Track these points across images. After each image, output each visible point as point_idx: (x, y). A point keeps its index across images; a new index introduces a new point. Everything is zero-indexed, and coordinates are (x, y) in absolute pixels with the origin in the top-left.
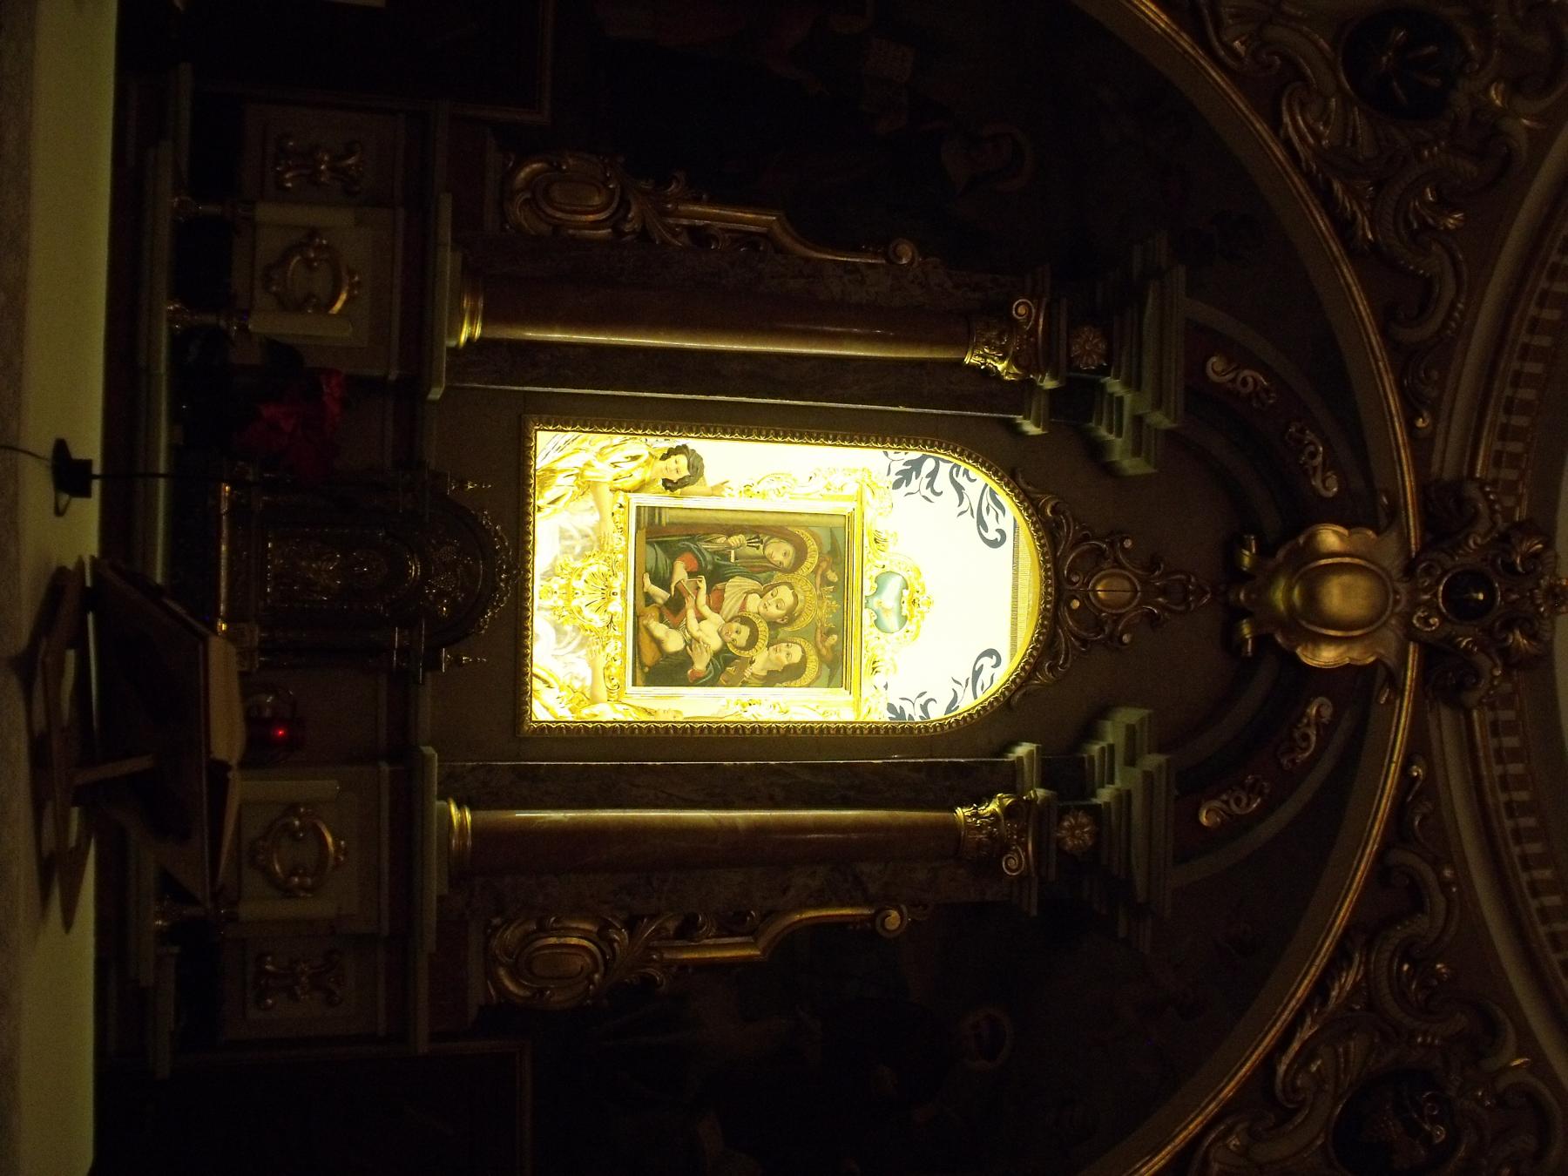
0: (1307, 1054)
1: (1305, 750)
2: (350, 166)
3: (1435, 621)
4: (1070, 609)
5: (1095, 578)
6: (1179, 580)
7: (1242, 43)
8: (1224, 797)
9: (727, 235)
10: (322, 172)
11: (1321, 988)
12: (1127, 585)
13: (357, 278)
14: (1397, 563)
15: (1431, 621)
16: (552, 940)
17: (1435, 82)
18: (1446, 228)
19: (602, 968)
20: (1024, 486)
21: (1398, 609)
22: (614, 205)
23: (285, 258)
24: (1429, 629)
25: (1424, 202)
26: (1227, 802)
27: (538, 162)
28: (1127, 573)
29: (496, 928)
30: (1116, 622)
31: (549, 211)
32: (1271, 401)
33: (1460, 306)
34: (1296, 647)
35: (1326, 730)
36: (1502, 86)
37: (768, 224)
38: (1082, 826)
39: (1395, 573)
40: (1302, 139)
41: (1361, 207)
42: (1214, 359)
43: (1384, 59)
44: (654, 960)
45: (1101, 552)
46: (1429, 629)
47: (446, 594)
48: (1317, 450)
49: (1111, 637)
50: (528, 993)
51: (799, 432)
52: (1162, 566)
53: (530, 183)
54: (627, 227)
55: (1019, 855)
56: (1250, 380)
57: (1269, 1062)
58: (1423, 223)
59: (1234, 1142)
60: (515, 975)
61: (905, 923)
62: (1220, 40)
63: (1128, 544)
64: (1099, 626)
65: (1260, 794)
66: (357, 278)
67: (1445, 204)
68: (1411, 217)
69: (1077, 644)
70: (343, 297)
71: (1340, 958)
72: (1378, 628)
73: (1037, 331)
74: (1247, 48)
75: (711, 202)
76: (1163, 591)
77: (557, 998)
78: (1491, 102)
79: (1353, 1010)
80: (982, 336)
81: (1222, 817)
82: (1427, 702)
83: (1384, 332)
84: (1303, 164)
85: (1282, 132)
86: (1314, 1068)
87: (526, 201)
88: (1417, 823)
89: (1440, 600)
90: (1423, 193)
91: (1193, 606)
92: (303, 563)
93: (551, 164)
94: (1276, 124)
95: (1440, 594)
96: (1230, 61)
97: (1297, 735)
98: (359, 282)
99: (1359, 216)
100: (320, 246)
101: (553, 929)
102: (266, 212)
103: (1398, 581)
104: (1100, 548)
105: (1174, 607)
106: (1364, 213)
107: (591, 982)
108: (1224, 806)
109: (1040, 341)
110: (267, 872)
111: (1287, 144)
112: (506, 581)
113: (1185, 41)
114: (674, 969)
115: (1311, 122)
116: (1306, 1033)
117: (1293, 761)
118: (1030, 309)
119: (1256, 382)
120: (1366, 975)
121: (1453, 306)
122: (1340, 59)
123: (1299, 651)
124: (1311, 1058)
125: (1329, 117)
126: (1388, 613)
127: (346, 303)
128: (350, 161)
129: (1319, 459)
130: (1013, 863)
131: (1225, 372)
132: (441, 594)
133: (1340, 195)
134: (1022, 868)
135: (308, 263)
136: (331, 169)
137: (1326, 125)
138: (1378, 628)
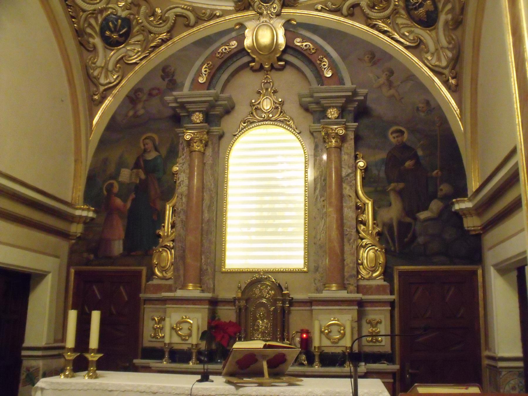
0: (403, 36)
1: (310, 46)
2: (158, 319)
3: (274, 6)
4: (272, 117)
5: (263, 110)
6: (264, 85)
7: (114, 75)
8: (323, 69)
9: (173, 218)
10: (160, 326)
11: (384, 32)
12: (266, 100)
13: (184, 317)
14: (255, 22)
15: (275, 7)
16: (365, 261)
17: (120, 21)
18: (161, 13)
19: (374, 247)
20: (238, 132)
21: (268, 21)
22: (166, 249)
23: (180, 336)
24: (277, 7)
25: (154, 20)
26: (325, 68)
27: (155, 269)
28: (262, 100)
29: (362, 277)
30: (276, 103)
31: (168, 266)
32: (211, 63)
33: (183, 6)
34: (280, 50)
35: (305, 39)
36: (119, 3)
37: (170, 207)
38: (331, 112)
39: (258, 22)
40: (139, 56)
41: (157, 37)
42: (200, 81)
43: (114, 37)
44: (372, 232)
45: (256, 108)
46: (277, 7)
47: (268, 291)
48: (224, 48)
49: (280, 104)
50: (380, 268)
51: (111, 260)
52: (259, 90)
53: (161, 272)
54: (172, 245)
55: (338, 130)
56: (205, 69)
57: (407, 47)
58: (160, 19)
59: (429, 58)
60: (374, 271)
61: (362, 160)
62: (113, 82)
63: (253, 101)
64: (277, 108)
65: (322, 58)
66: (184, 317)
67: (154, 14)
68: (158, 23)
69: (282, 114)
70: (189, 320)
71: (374, 27)
72: (273, 27)
73: (193, 133)
74: (115, 74)
75: (164, 223)
76: (267, 89)
77: (382, 260)
78: (124, 5)
79: (390, 23)
80: (195, 148)
81: (329, 70)
82: (299, 5)
83: (193, 27)
84: (147, 55)
85: (138, 62)
86: (407, 34)
87: (166, 273)
88: (334, 7)
89: (268, 4)
90: (151, 21)
91: (271, 81)
92: (260, 330)
93: (156, 266)
94: (136, 64)
95: (267, 5)
96: (119, 79)
97: (305, 48)
98: (185, 316)
99: (160, 38)
100: (176, 326)
101: (362, 261)
102: (167, 341)
103: (260, 21)
104: (255, 109)
105: (271, 86)
106: (159, 36)
107: (377, 250)
108: (326, 69)
109: (196, 131)
110: (339, 339)
111: (141, 60)
112: (264, 275)
113: (115, 92)
114: (375, 226)
115: (134, 54)
116: (396, 36)
117: (313, 49)
118: (187, 135)
119: (206, 68)
120: (378, 19)
121: (183, 8)
122: (116, 48)
123: (281, 50)
124: (404, 35)
125: (132, 49)
126: (269, 24)
127: (190, 319)
128: (156, 319)
129: (226, 47)
130: (341, 132)
131: (203, 77)
132: (268, 293)
133: (155, 43)
134: (342, 129)
135: (180, 329)
136: (158, 324)
137: (134, 50)
138: (273, 27)
